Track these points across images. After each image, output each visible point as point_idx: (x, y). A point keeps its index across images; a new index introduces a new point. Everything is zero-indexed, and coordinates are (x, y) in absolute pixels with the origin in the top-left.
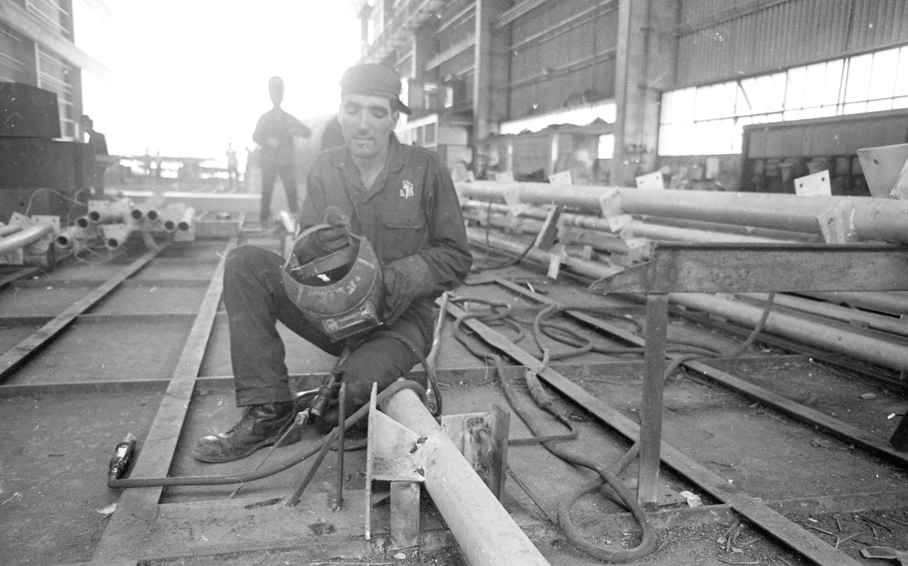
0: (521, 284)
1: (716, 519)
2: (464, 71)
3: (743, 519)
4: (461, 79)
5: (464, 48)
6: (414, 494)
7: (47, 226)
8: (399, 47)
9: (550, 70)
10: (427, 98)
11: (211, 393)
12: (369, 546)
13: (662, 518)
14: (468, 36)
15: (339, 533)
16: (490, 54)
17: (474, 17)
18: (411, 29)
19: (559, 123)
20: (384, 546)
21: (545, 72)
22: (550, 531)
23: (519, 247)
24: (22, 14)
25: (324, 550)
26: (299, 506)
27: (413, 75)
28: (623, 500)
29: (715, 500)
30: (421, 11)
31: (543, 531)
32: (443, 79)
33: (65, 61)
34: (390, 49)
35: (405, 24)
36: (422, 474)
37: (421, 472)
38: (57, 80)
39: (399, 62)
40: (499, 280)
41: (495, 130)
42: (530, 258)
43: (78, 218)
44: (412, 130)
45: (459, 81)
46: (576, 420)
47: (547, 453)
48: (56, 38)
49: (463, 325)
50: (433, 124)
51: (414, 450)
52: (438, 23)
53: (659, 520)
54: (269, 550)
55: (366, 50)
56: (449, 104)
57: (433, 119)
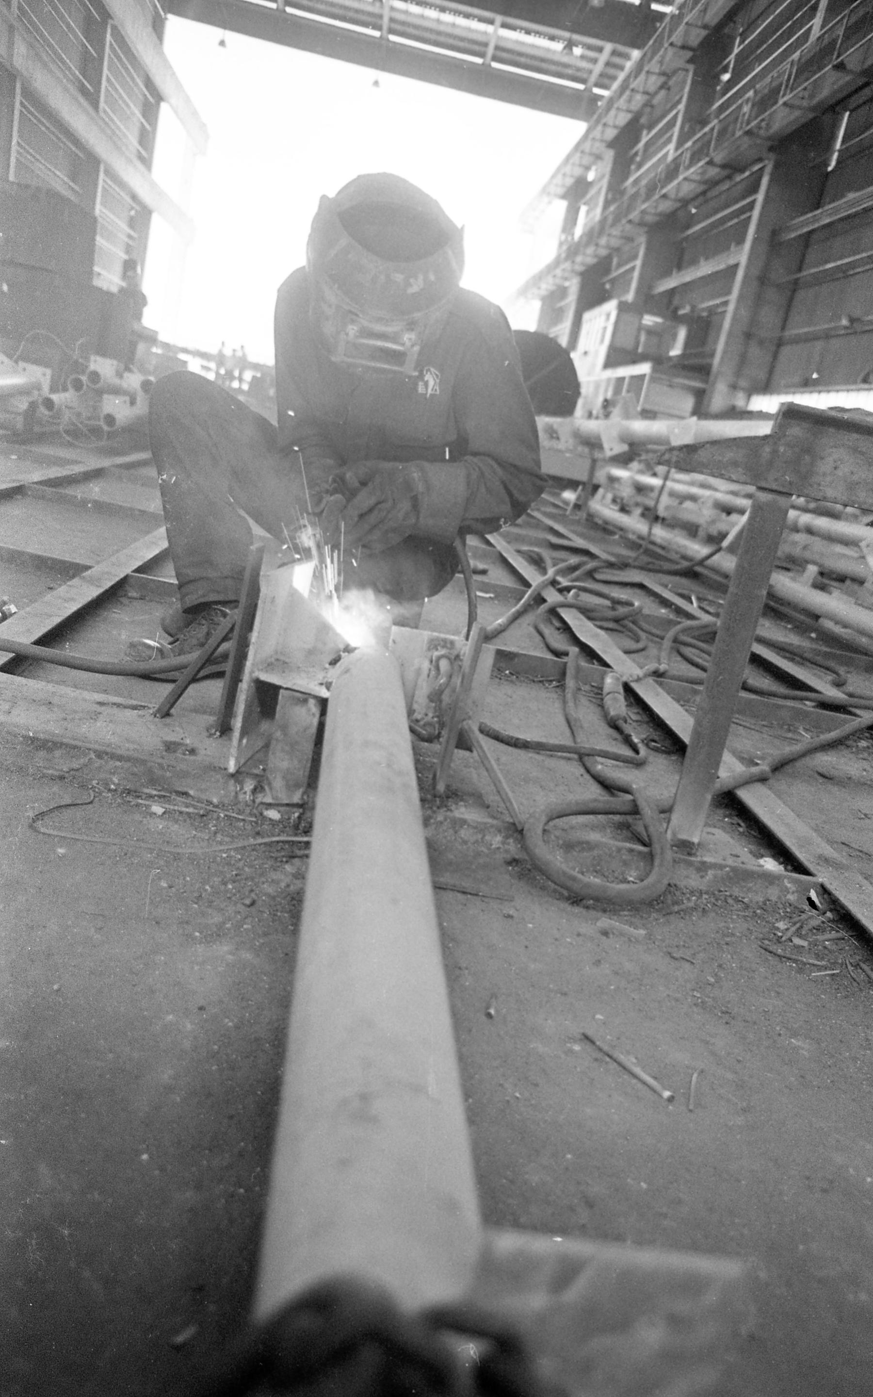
0: (682, 596)
1: (791, 898)
2: (711, 303)
3: (834, 904)
4: (705, 314)
5: (722, 266)
6: (307, 716)
7: (34, 380)
8: (618, 250)
9: (852, 320)
10: (643, 338)
11: (142, 598)
12: (232, 785)
13: (699, 870)
14: (733, 248)
15: (199, 758)
16: (761, 280)
17: (750, 217)
18: (641, 224)
19: (848, 407)
20: (254, 791)
21: (845, 322)
22: (511, 841)
23: (698, 549)
24: (92, 119)
25: (168, 774)
26: (168, 720)
27: (630, 297)
28: (648, 836)
29: (799, 868)
30: (664, 196)
31: (499, 838)
32: (676, 309)
33: (134, 197)
34: (603, 252)
35: (634, 215)
36: (328, 688)
37: (328, 686)
38: (119, 222)
39: (614, 274)
40: (647, 583)
41: (740, 401)
42: (713, 569)
43: (73, 376)
44: (609, 380)
45: (700, 318)
46: (656, 750)
47: (582, 770)
48: (130, 161)
49: (553, 612)
50: (642, 377)
51: (334, 662)
52: (691, 221)
53: (692, 873)
54: (95, 751)
55: (565, 247)
56: (676, 351)
57: (644, 368)
